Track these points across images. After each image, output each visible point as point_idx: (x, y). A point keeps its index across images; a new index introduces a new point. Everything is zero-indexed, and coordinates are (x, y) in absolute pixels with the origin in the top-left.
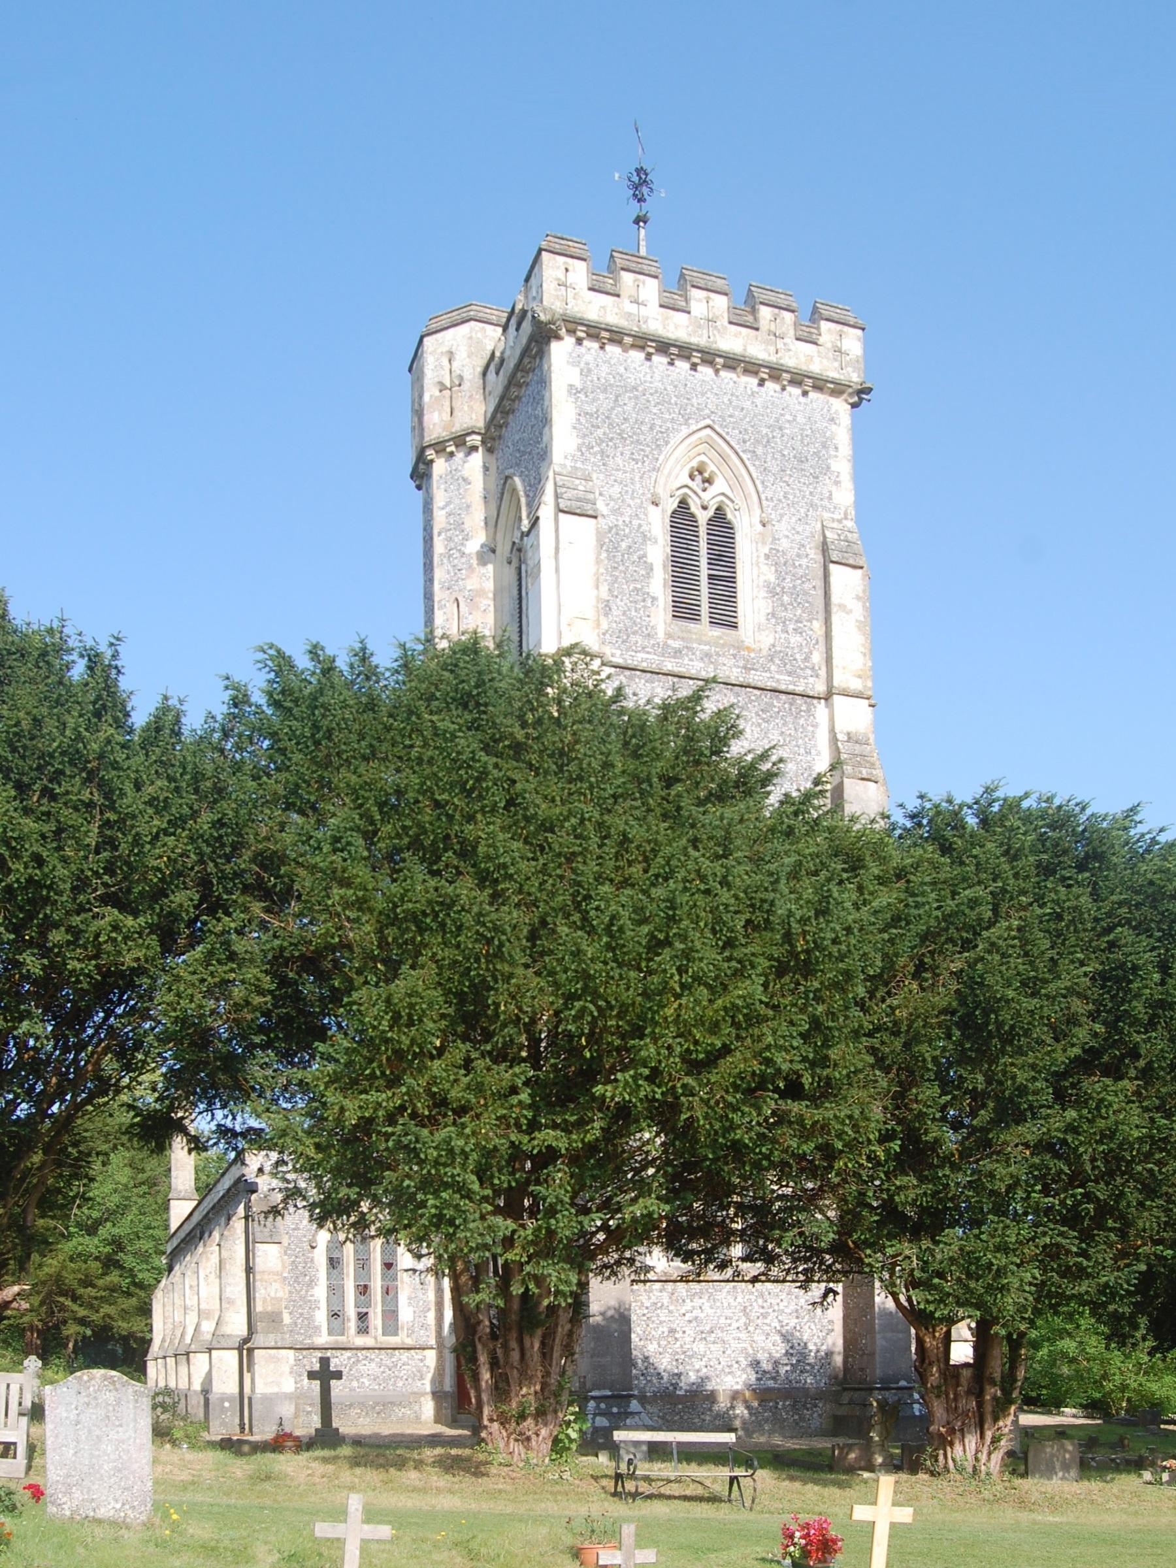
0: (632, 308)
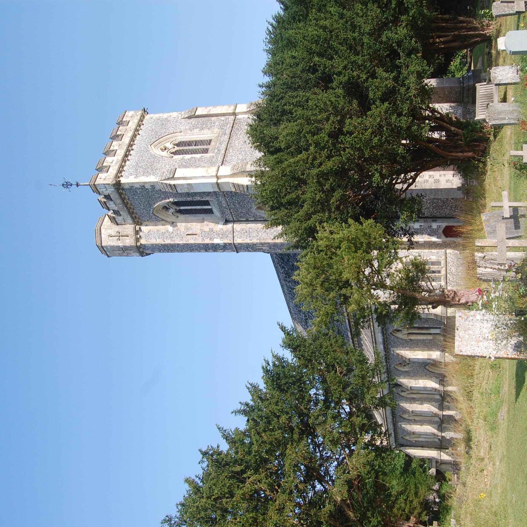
0: (114, 163)
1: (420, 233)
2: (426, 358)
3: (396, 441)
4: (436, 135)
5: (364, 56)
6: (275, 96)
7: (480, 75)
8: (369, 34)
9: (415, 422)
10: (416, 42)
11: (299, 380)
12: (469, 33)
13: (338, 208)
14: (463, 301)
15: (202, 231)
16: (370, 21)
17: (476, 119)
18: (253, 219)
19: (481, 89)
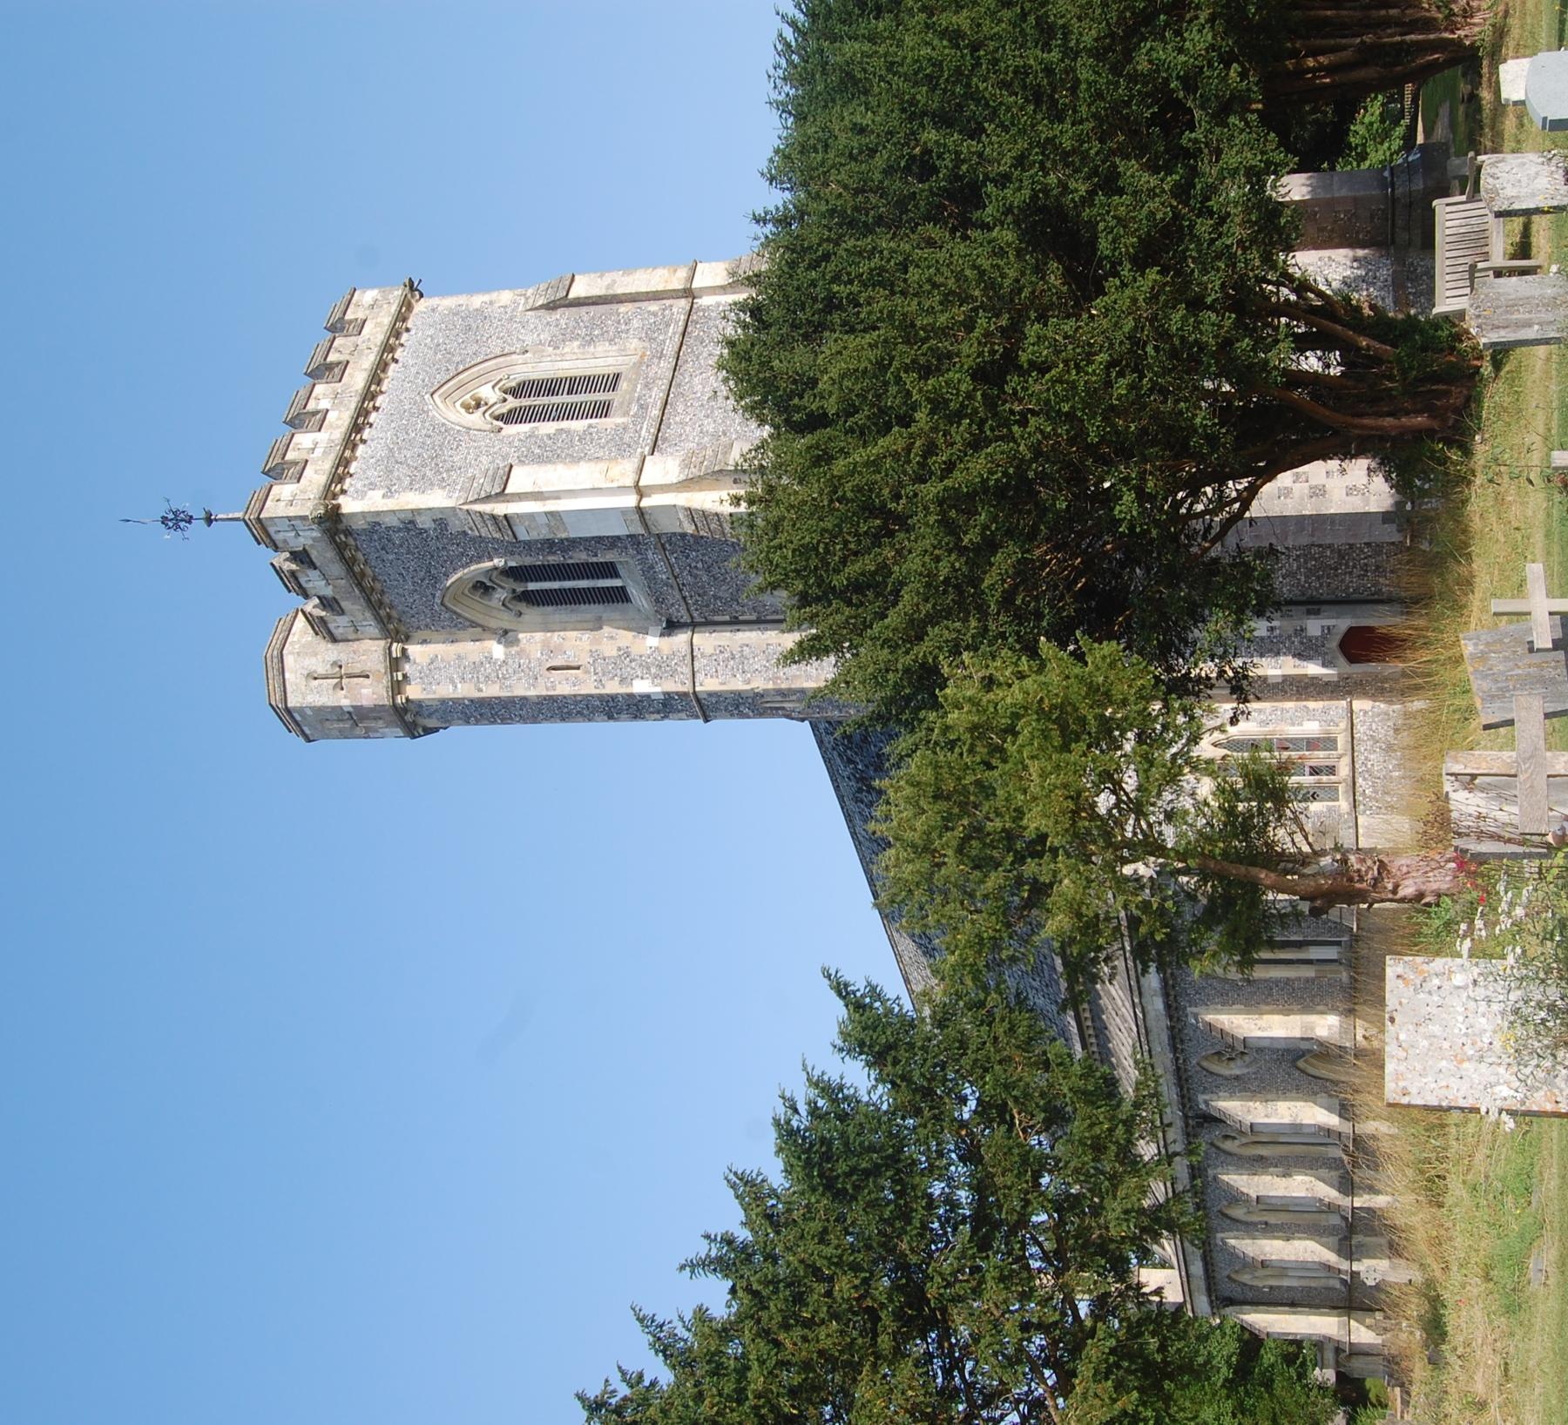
0: (319, 452)
1: (1270, 651)
2: (1298, 1035)
4: (1311, 362)
5: (1081, 123)
6: (805, 250)
7: (1444, 169)
8: (1091, 52)
9: (1269, 1230)
10: (1243, 75)
11: (894, 1159)
12: (1408, 38)
13: (1007, 600)
15: (596, 656)
16: (1098, 11)
17: (1435, 311)
18: (754, 617)
19: (1450, 215)
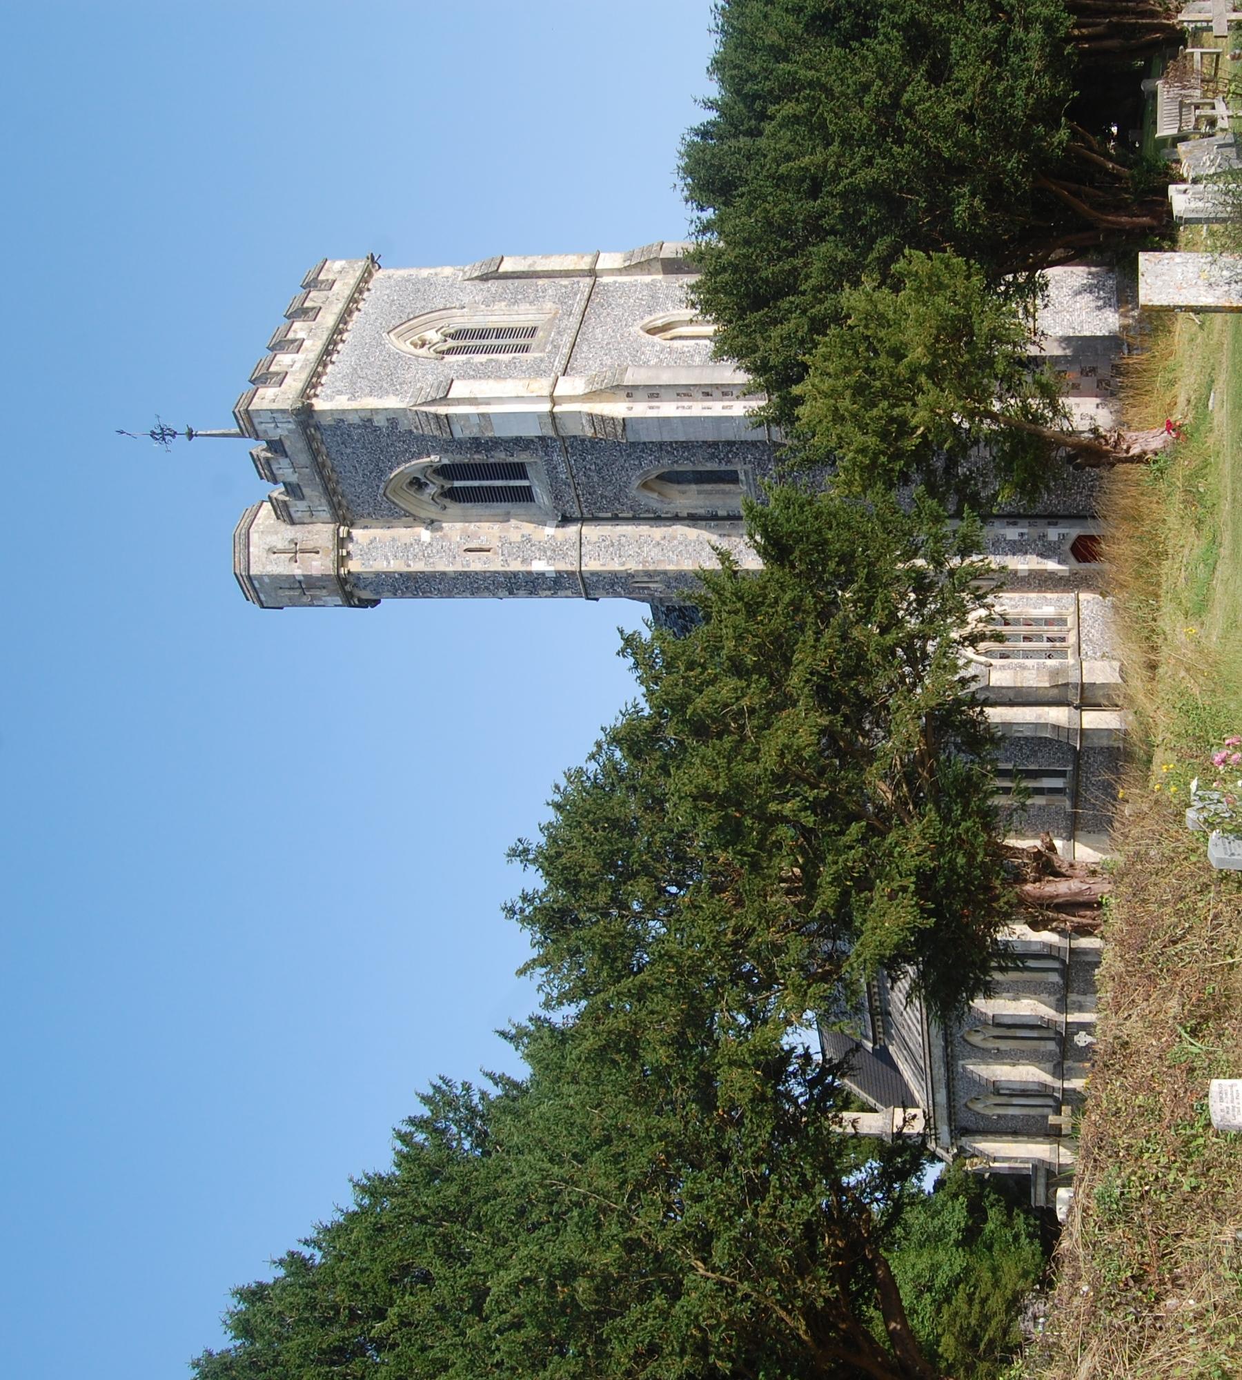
0: (297, 366)
1: (1020, 551)
3: (950, 1119)
14: (1135, 450)
15: (504, 541)
18: (630, 515)
